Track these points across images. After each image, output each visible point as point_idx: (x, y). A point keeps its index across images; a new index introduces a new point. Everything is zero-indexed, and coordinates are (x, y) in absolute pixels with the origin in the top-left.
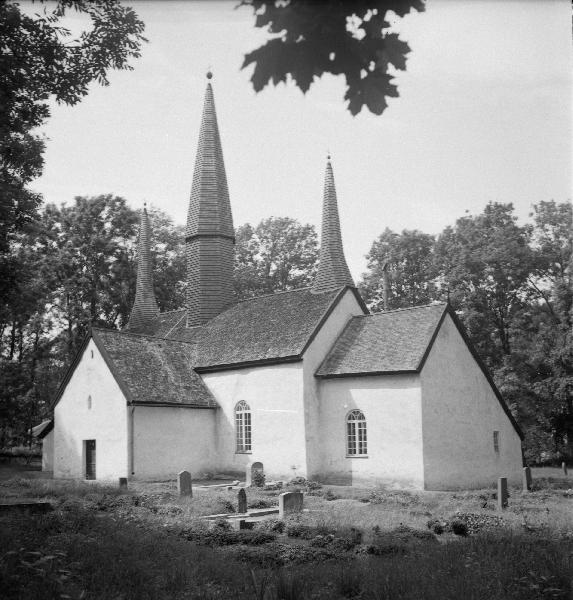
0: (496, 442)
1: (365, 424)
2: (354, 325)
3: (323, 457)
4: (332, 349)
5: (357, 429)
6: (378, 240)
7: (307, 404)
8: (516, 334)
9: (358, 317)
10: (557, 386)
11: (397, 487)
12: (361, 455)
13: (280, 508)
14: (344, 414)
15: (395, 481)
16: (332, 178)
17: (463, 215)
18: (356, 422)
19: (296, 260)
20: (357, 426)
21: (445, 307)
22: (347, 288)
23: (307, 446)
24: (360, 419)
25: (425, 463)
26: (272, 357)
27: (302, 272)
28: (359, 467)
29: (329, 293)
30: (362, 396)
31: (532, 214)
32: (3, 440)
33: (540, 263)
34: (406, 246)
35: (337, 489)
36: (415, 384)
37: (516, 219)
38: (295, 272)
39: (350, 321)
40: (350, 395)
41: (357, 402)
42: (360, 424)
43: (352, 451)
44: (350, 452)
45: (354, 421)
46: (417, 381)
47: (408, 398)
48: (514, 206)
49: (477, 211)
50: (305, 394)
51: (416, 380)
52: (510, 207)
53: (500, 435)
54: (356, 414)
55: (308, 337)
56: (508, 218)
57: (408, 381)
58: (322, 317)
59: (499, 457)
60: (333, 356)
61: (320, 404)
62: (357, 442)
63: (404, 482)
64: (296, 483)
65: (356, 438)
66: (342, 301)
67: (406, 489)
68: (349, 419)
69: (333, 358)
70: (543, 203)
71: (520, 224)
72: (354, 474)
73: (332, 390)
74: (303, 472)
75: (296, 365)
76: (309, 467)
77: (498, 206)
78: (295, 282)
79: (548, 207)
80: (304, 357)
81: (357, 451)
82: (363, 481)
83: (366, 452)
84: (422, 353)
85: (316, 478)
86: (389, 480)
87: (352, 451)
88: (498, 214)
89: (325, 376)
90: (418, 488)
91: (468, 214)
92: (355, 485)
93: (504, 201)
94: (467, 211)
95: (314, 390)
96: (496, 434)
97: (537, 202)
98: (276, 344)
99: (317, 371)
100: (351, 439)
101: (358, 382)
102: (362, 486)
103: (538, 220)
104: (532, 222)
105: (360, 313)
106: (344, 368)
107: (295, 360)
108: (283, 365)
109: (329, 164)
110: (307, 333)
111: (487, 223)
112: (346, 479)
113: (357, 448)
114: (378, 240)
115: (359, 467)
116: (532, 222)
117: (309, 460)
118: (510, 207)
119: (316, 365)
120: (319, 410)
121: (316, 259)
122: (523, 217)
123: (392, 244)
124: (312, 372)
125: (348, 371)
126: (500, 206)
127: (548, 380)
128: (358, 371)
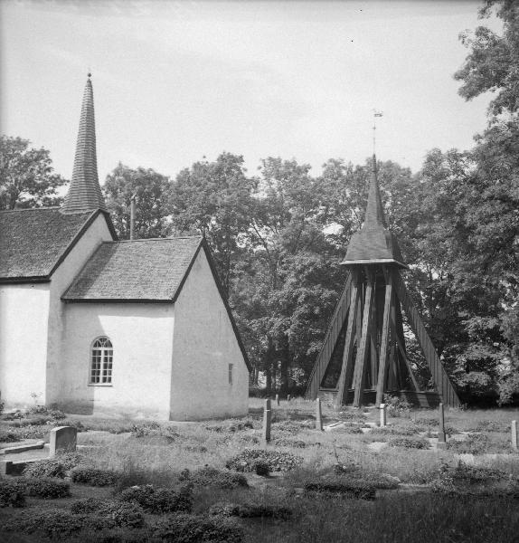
0: (230, 373)
1: (111, 352)
2: (103, 253)
3: (64, 384)
4: (81, 272)
5: (103, 356)
6: (112, 174)
7: (51, 328)
8: (240, 274)
9: (107, 243)
10: (272, 324)
11: (141, 417)
12: (106, 384)
13: (51, 445)
14: (90, 340)
15: (139, 411)
16: (92, 97)
17: (201, 160)
18: (103, 349)
19: (30, 185)
20: (103, 353)
21: (200, 240)
22: (100, 211)
23: (47, 372)
24: (106, 346)
25: (172, 393)
26: (15, 275)
27: (31, 197)
28: (102, 396)
29: (80, 215)
30: (111, 324)
31: (260, 168)
32: (3, 171)
33: (262, 213)
34: (139, 184)
35: (87, 420)
36: (169, 313)
37: (246, 170)
38: (26, 196)
39: (100, 246)
40: (99, 321)
41: (104, 328)
42: (106, 352)
43: (95, 379)
44: (93, 380)
45: (100, 349)
46: (171, 311)
47: (161, 326)
48: (244, 158)
49: (212, 159)
50: (50, 317)
51: (169, 309)
52: (241, 159)
53: (234, 368)
54: (103, 341)
55: (57, 257)
56: (238, 169)
57: (161, 310)
58: (73, 239)
59: (231, 388)
60: (82, 279)
61: (65, 328)
62: (102, 370)
63: (147, 412)
64: (37, 412)
65: (101, 364)
66: (94, 224)
67: (151, 419)
68: (95, 346)
69: (83, 280)
70: (270, 159)
71: (248, 175)
72: (96, 404)
73: (77, 313)
74: (42, 400)
75: (43, 286)
76: (47, 398)
77: (230, 156)
78: (26, 205)
79: (274, 162)
80: (52, 278)
81: (101, 380)
82: (104, 410)
83: (110, 380)
84: (178, 283)
85: (54, 406)
86: (132, 409)
87: (95, 379)
88: (230, 164)
89: (72, 300)
90: (163, 419)
91: (205, 160)
92: (96, 414)
93: (236, 153)
94: (204, 157)
95: (59, 313)
96: (231, 366)
97: (265, 157)
98: (20, 263)
99: (64, 294)
100: (95, 364)
101: (108, 309)
102: (104, 416)
103: (265, 173)
104: (259, 174)
105: (111, 239)
106: (94, 293)
107: (43, 281)
108: (28, 285)
109: (89, 82)
110: (56, 254)
111: (219, 170)
112: (87, 408)
113: (101, 376)
114: (112, 174)
115: (102, 396)
116: (259, 174)
117: (48, 387)
118: (241, 159)
119: (65, 287)
120: (63, 336)
121: (48, 185)
122: (251, 170)
123: (126, 176)
124: (59, 296)
125: (98, 296)
126: (232, 157)
127: (264, 319)
128: (109, 297)
